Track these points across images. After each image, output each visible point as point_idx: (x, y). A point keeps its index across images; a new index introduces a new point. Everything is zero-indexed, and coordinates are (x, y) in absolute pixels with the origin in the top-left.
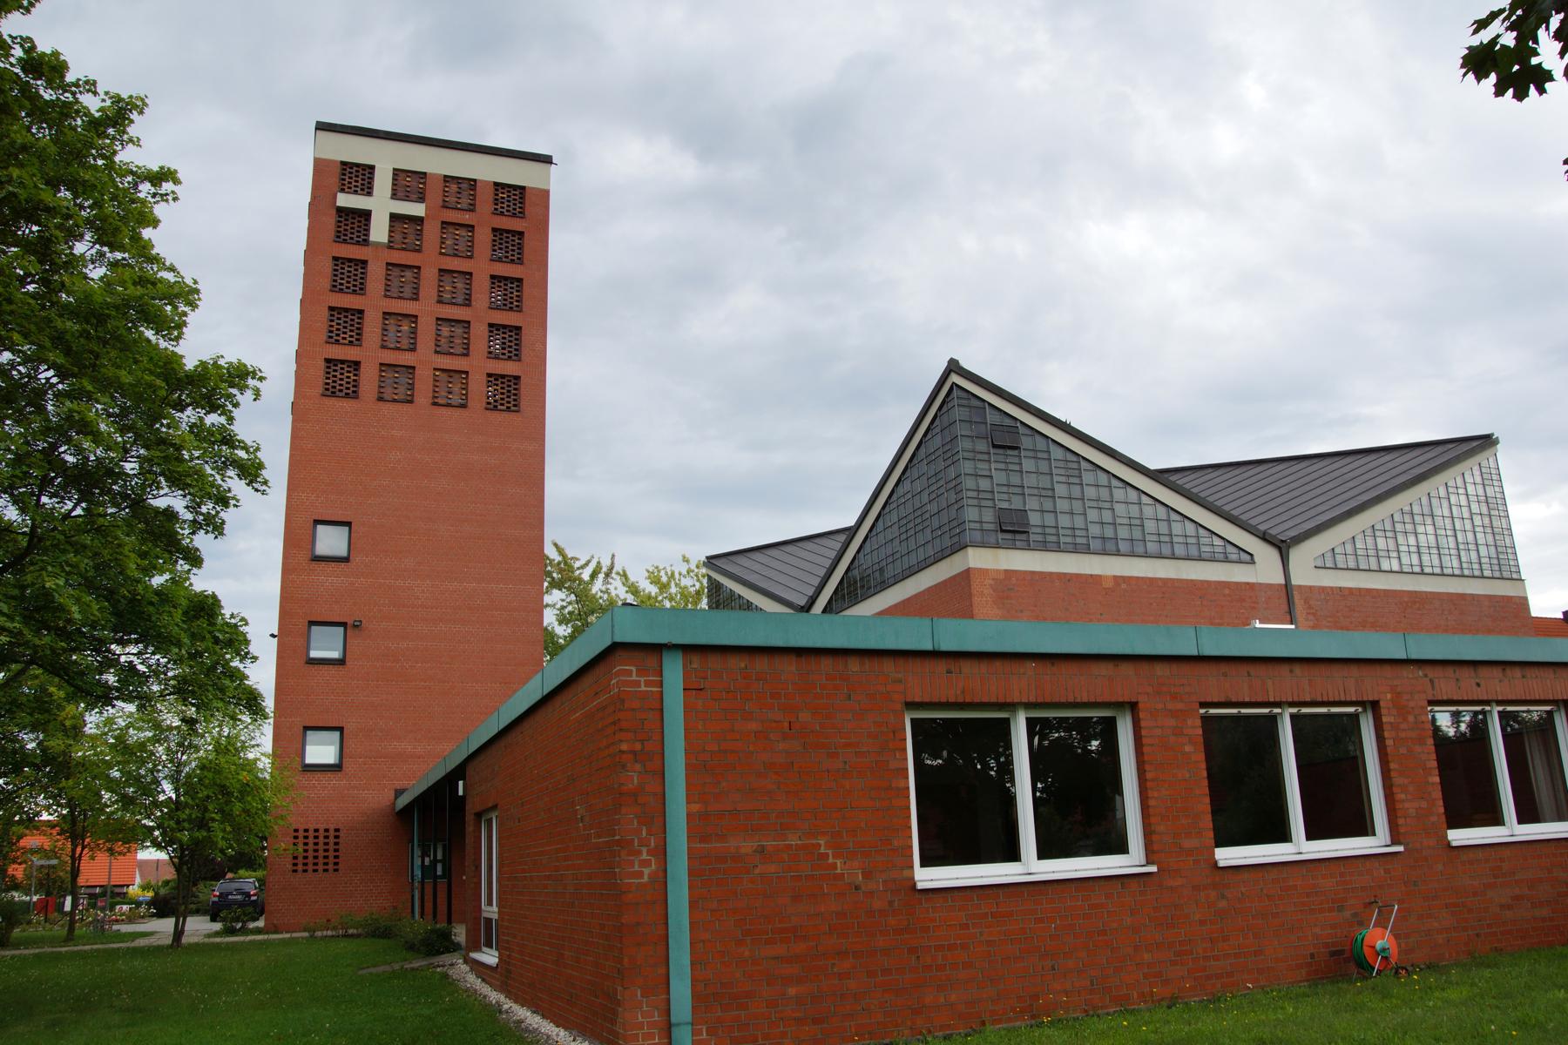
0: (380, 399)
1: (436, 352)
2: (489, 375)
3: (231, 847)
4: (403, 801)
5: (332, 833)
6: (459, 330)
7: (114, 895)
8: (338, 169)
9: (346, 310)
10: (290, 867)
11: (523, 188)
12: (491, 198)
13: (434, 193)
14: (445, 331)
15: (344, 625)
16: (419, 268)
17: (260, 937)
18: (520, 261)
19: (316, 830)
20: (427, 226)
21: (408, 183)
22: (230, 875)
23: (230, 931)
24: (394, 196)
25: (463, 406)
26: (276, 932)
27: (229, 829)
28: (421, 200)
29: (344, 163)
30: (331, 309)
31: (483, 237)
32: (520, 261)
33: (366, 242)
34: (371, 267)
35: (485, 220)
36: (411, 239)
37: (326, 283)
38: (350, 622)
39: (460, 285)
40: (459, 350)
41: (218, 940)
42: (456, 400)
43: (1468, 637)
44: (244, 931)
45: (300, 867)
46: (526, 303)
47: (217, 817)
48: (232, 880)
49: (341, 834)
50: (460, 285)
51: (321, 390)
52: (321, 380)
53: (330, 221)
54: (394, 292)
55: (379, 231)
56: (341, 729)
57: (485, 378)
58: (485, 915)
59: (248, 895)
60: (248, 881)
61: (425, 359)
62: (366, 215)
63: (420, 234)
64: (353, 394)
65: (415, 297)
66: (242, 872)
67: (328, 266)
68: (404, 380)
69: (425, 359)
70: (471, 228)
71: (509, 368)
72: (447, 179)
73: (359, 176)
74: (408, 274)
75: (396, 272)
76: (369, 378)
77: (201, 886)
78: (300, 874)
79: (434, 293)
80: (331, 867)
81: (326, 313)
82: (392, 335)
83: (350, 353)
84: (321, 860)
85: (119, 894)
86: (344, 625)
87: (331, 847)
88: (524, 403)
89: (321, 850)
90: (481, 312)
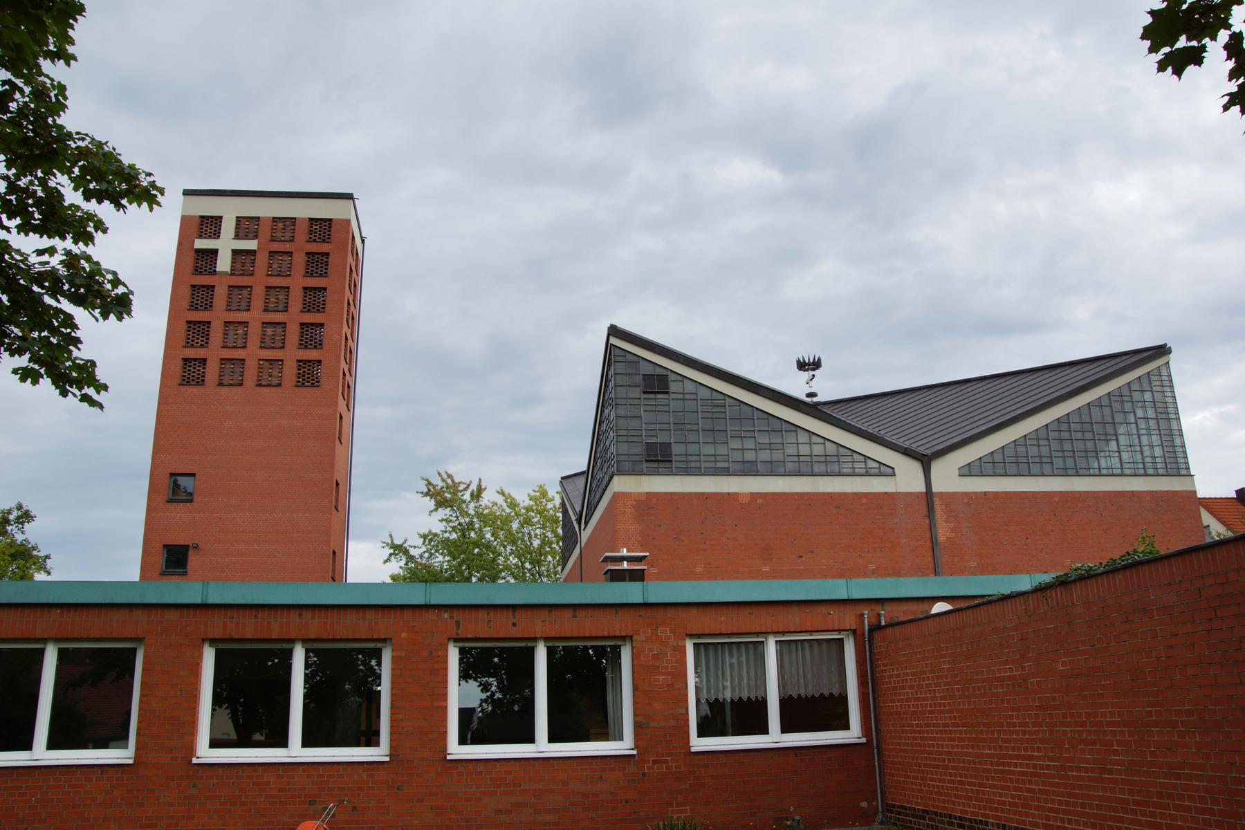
2: (299, 361)
9: (199, 322)
13: (265, 232)
21: (246, 226)
25: (279, 385)
29: (202, 217)
35: (301, 246)
37: (185, 304)
42: (275, 381)
53: (190, 260)
54: (234, 306)
55: (224, 264)
61: (253, 353)
64: (201, 382)
70: (290, 253)
71: (313, 354)
75: (236, 292)
81: (185, 326)
82: (231, 336)
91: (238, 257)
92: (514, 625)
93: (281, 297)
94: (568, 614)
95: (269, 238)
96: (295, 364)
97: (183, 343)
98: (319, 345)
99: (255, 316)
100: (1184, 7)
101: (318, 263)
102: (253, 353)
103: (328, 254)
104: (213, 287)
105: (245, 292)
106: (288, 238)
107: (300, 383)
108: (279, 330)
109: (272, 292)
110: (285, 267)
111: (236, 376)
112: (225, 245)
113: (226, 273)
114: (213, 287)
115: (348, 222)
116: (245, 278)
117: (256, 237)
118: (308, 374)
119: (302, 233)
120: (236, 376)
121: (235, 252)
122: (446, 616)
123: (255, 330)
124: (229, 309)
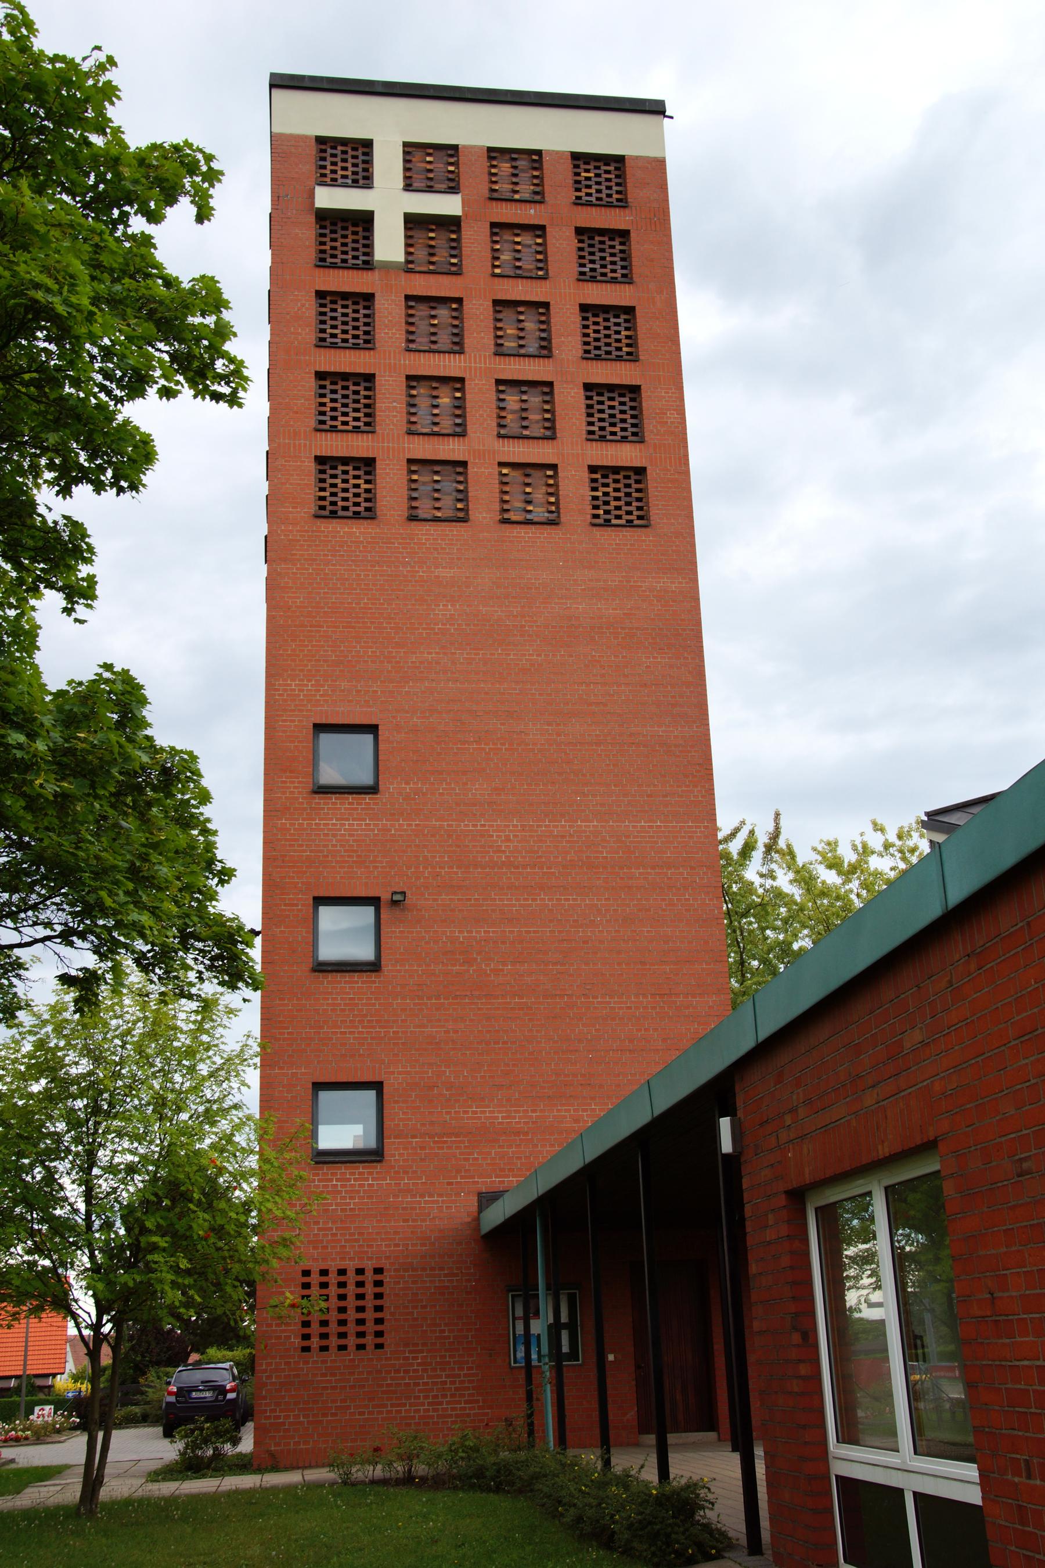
0: (413, 518)
1: (500, 436)
2: (593, 469)
3: (189, 1304)
4: (496, 1215)
5: (369, 1277)
6: (535, 399)
7: (34, 1389)
8: (313, 149)
10: (297, 1342)
11: (620, 160)
12: (570, 180)
13: (474, 175)
14: (512, 400)
15: (373, 901)
16: (459, 301)
17: (247, 1481)
18: (627, 279)
19: (342, 1272)
21: (430, 164)
22: (194, 1357)
23: (190, 1466)
25: (553, 523)
26: (275, 1468)
27: (184, 1264)
28: (453, 189)
29: (321, 140)
30: (320, 376)
31: (562, 245)
32: (627, 279)
33: (368, 265)
34: (379, 303)
35: (561, 215)
36: (442, 256)
37: (309, 334)
38: (385, 896)
39: (530, 325)
40: (537, 431)
41: (168, 1488)
44: (218, 1465)
45: (315, 1342)
46: (650, 426)
47: (162, 1242)
48: (197, 1365)
49: (386, 1278)
50: (530, 325)
51: (313, 509)
52: (311, 492)
53: (307, 234)
54: (422, 342)
55: (389, 244)
56: (377, 1086)
57: (586, 475)
58: (839, 1469)
59: (222, 1390)
60: (218, 1370)
61: (483, 447)
62: (364, 221)
63: (456, 247)
65: (458, 347)
66: (212, 1351)
67: (309, 307)
68: (448, 486)
69: (483, 447)
70: (539, 230)
71: (625, 455)
72: (494, 153)
73: (349, 159)
74: (443, 313)
75: (421, 311)
76: (391, 484)
77: (152, 1375)
78: (315, 1356)
79: (489, 341)
80: (369, 1340)
81: (312, 383)
83: (357, 446)
84: (351, 1328)
85: (41, 1388)
86: (373, 901)
87: (369, 1302)
88: (655, 512)
89: (354, 1309)
90: (570, 369)
95: (486, 193)
100: (7, 133)
116: (445, 280)
119: (559, 182)
121: (413, 222)
124: (410, 344)
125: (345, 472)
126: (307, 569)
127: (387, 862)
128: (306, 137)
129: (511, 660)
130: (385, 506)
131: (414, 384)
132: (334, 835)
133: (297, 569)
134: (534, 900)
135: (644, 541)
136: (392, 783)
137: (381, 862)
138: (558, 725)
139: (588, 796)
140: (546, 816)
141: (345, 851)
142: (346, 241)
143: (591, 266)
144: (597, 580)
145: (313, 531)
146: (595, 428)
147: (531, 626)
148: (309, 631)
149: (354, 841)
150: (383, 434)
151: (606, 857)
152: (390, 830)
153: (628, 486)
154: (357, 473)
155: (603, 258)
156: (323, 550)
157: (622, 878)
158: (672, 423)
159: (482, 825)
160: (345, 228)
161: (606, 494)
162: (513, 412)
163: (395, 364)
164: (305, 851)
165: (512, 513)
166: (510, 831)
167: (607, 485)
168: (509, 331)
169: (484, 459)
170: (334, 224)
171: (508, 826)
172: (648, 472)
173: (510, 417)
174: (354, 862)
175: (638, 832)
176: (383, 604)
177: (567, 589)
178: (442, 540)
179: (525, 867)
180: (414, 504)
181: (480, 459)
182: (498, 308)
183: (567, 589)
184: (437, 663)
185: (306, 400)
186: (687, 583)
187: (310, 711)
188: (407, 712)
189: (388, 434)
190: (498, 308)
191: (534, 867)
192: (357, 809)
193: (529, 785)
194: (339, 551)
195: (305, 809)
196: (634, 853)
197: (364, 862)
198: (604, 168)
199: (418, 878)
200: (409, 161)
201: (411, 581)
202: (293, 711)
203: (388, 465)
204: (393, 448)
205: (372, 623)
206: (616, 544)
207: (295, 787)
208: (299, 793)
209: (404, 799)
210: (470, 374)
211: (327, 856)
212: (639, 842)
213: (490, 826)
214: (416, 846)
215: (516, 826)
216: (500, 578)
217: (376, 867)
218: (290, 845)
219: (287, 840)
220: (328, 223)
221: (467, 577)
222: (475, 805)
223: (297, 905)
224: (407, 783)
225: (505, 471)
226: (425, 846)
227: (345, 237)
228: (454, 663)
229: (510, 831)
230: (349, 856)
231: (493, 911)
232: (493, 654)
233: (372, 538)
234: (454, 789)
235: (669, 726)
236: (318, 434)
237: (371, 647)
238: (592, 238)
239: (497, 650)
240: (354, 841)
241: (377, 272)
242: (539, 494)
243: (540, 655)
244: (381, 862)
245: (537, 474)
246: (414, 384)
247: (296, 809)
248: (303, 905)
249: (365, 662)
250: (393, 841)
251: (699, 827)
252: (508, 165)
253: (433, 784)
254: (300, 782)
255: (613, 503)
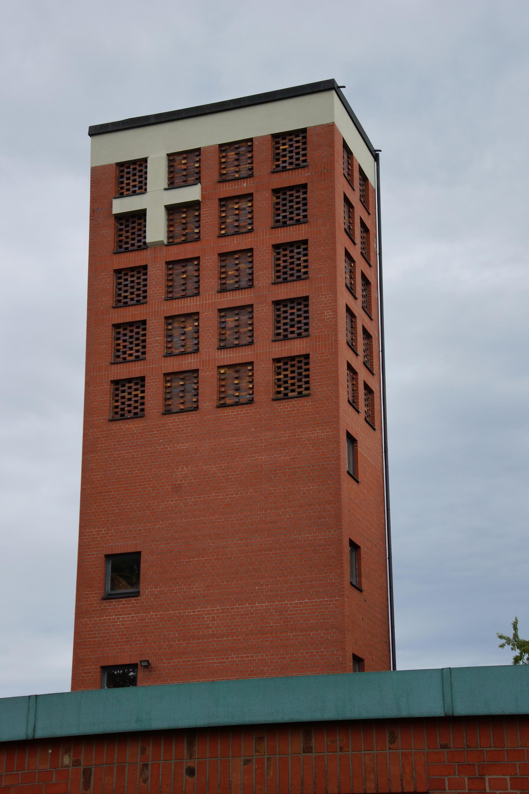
9: (131, 324)
13: (210, 169)
20: (204, 210)
21: (183, 166)
24: (172, 158)
25: (251, 402)
29: (120, 165)
33: (144, 247)
34: (151, 271)
35: (263, 184)
37: (109, 300)
42: (245, 396)
43: (507, 713)
53: (109, 233)
54: (178, 291)
55: (156, 230)
64: (139, 414)
70: (249, 196)
71: (296, 347)
72: (223, 148)
75: (178, 269)
82: (177, 339)
91: (176, 217)
92: (191, 772)
93: (242, 266)
94: (294, 745)
95: (216, 177)
96: (270, 367)
97: (110, 358)
98: (303, 333)
99: (208, 302)
101: (291, 203)
102: (209, 358)
103: (304, 186)
104: (145, 267)
105: (190, 268)
106: (244, 173)
107: (281, 396)
108: (244, 318)
109: (230, 261)
110: (244, 217)
111: (189, 397)
112: (155, 200)
113: (159, 244)
114: (145, 267)
115: (331, 128)
117: (198, 180)
118: (294, 377)
120: (189, 397)
122: (67, 760)
123: (209, 323)
125: (130, 388)
126: (104, 456)
127: (143, 640)
128: (110, 165)
129: (220, 499)
130: (149, 407)
131: (170, 321)
132: (114, 626)
133: (99, 456)
134: (227, 658)
135: (306, 406)
136: (147, 589)
137: (139, 641)
138: (247, 539)
139: (263, 585)
140: (237, 601)
141: (120, 635)
142: (134, 230)
143: (284, 214)
144: (275, 438)
145: (108, 430)
146: (281, 331)
147: (233, 475)
148: (104, 496)
149: (125, 628)
150: (150, 359)
151: (273, 626)
152: (145, 619)
153: (300, 368)
154: (136, 387)
155: (291, 207)
156: (114, 442)
157: (282, 640)
158: (328, 319)
159: (198, 611)
160: (134, 222)
161: (286, 376)
162: (231, 329)
163: (158, 311)
164: (97, 637)
165: (227, 399)
166: (215, 614)
167: (286, 370)
168: (230, 273)
169: (209, 366)
170: (127, 221)
171: (214, 610)
172: (311, 356)
173: (228, 332)
174: (124, 642)
175: (293, 607)
176: (146, 472)
177: (256, 447)
178: (182, 425)
179: (223, 637)
180: (168, 403)
181: (206, 367)
182: (222, 259)
183: (256, 447)
184: (177, 507)
185: (106, 344)
186: (332, 431)
187: (103, 547)
188: (158, 541)
189: (153, 359)
190: (222, 259)
191: (227, 637)
192: (127, 607)
193: (228, 581)
194: (122, 441)
195: (98, 610)
196: (290, 622)
197: (130, 641)
198: (295, 139)
199: (160, 649)
200: (172, 166)
201: (163, 455)
202: (94, 548)
203: (152, 379)
204: (156, 367)
205: (139, 485)
206: (288, 411)
207: (93, 597)
208: (95, 600)
209: (154, 598)
210: (203, 310)
211: (109, 640)
212: (294, 614)
213: (203, 611)
214: (160, 628)
215: (219, 610)
216: (215, 445)
217: (136, 644)
218: (89, 635)
219: (87, 631)
220: (124, 221)
221: (196, 448)
222: (195, 598)
223: (91, 672)
224: (156, 588)
225: (222, 371)
226: (165, 628)
227: (133, 228)
228: (186, 506)
229: (215, 614)
230: (121, 638)
231: (203, 667)
232: (209, 497)
233: (141, 429)
234: (183, 589)
235: (316, 533)
236: (113, 366)
237: (139, 501)
238: (285, 194)
239: (212, 493)
240: (125, 628)
241: (149, 250)
242: (244, 384)
243: (237, 494)
244: (139, 641)
245: (243, 369)
246: (170, 321)
247: (93, 611)
248: (94, 672)
249: (136, 511)
250: (147, 626)
251: (332, 601)
252: (233, 153)
253: (171, 586)
254: (96, 593)
255: (290, 382)
